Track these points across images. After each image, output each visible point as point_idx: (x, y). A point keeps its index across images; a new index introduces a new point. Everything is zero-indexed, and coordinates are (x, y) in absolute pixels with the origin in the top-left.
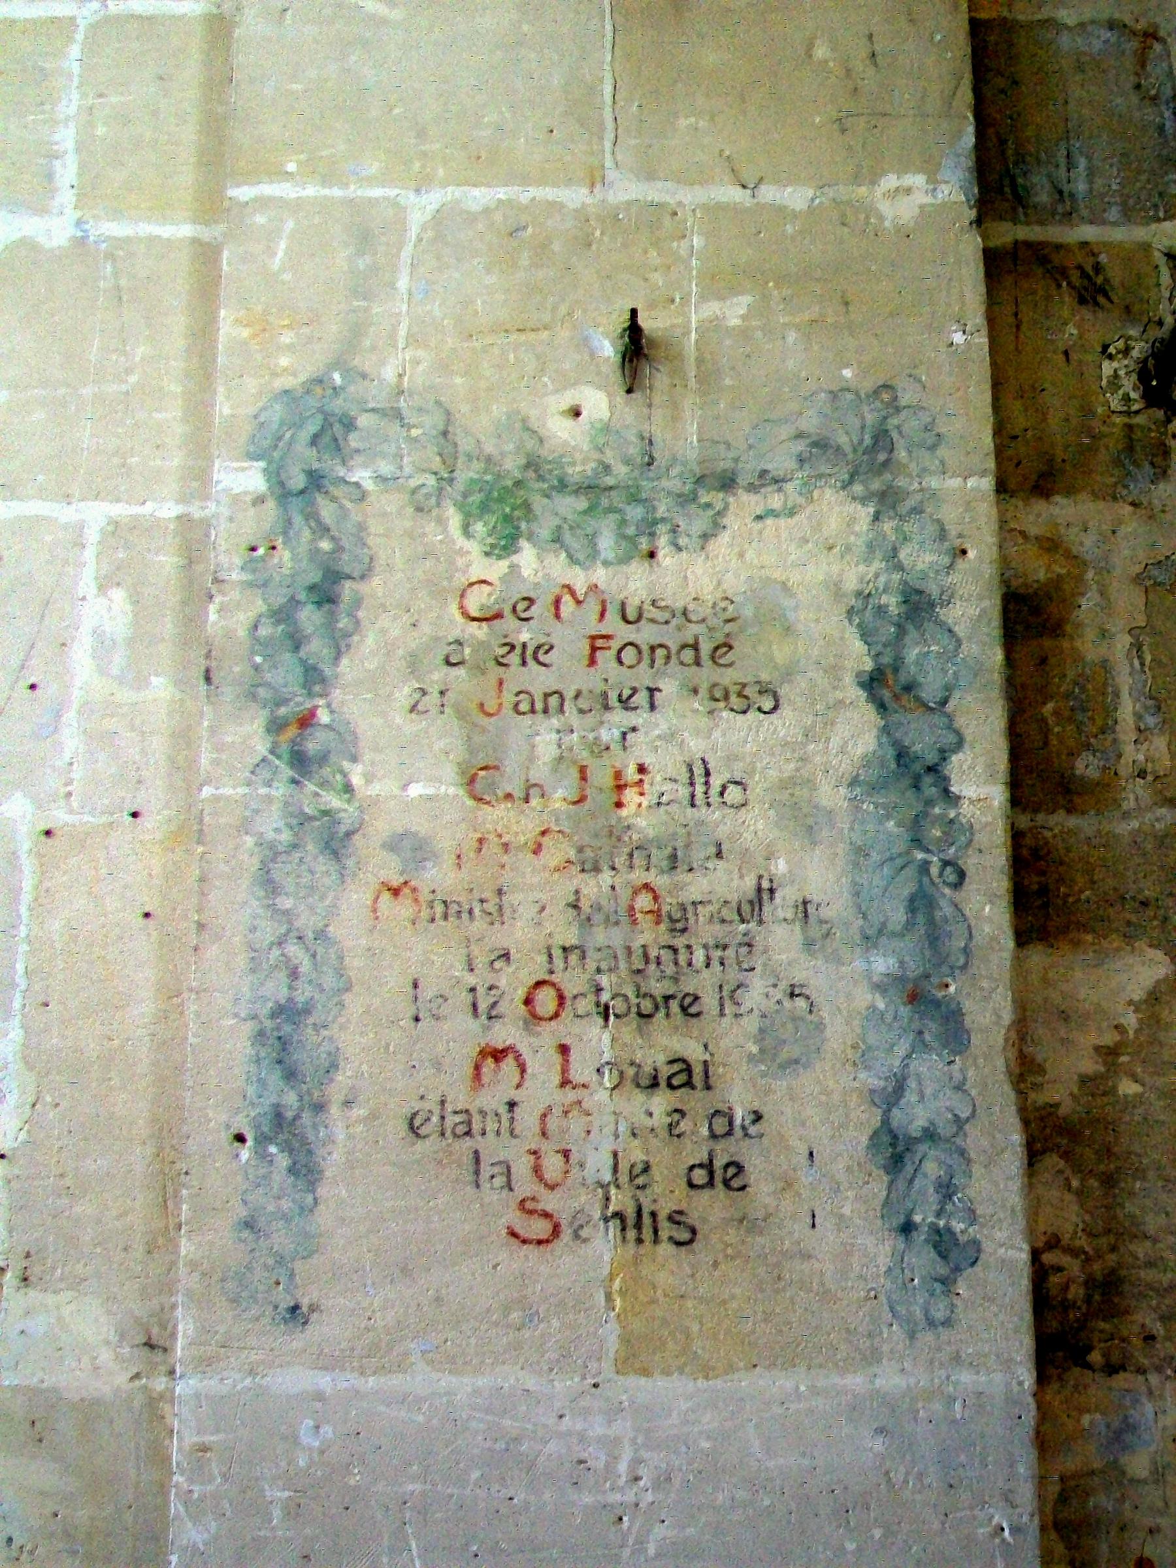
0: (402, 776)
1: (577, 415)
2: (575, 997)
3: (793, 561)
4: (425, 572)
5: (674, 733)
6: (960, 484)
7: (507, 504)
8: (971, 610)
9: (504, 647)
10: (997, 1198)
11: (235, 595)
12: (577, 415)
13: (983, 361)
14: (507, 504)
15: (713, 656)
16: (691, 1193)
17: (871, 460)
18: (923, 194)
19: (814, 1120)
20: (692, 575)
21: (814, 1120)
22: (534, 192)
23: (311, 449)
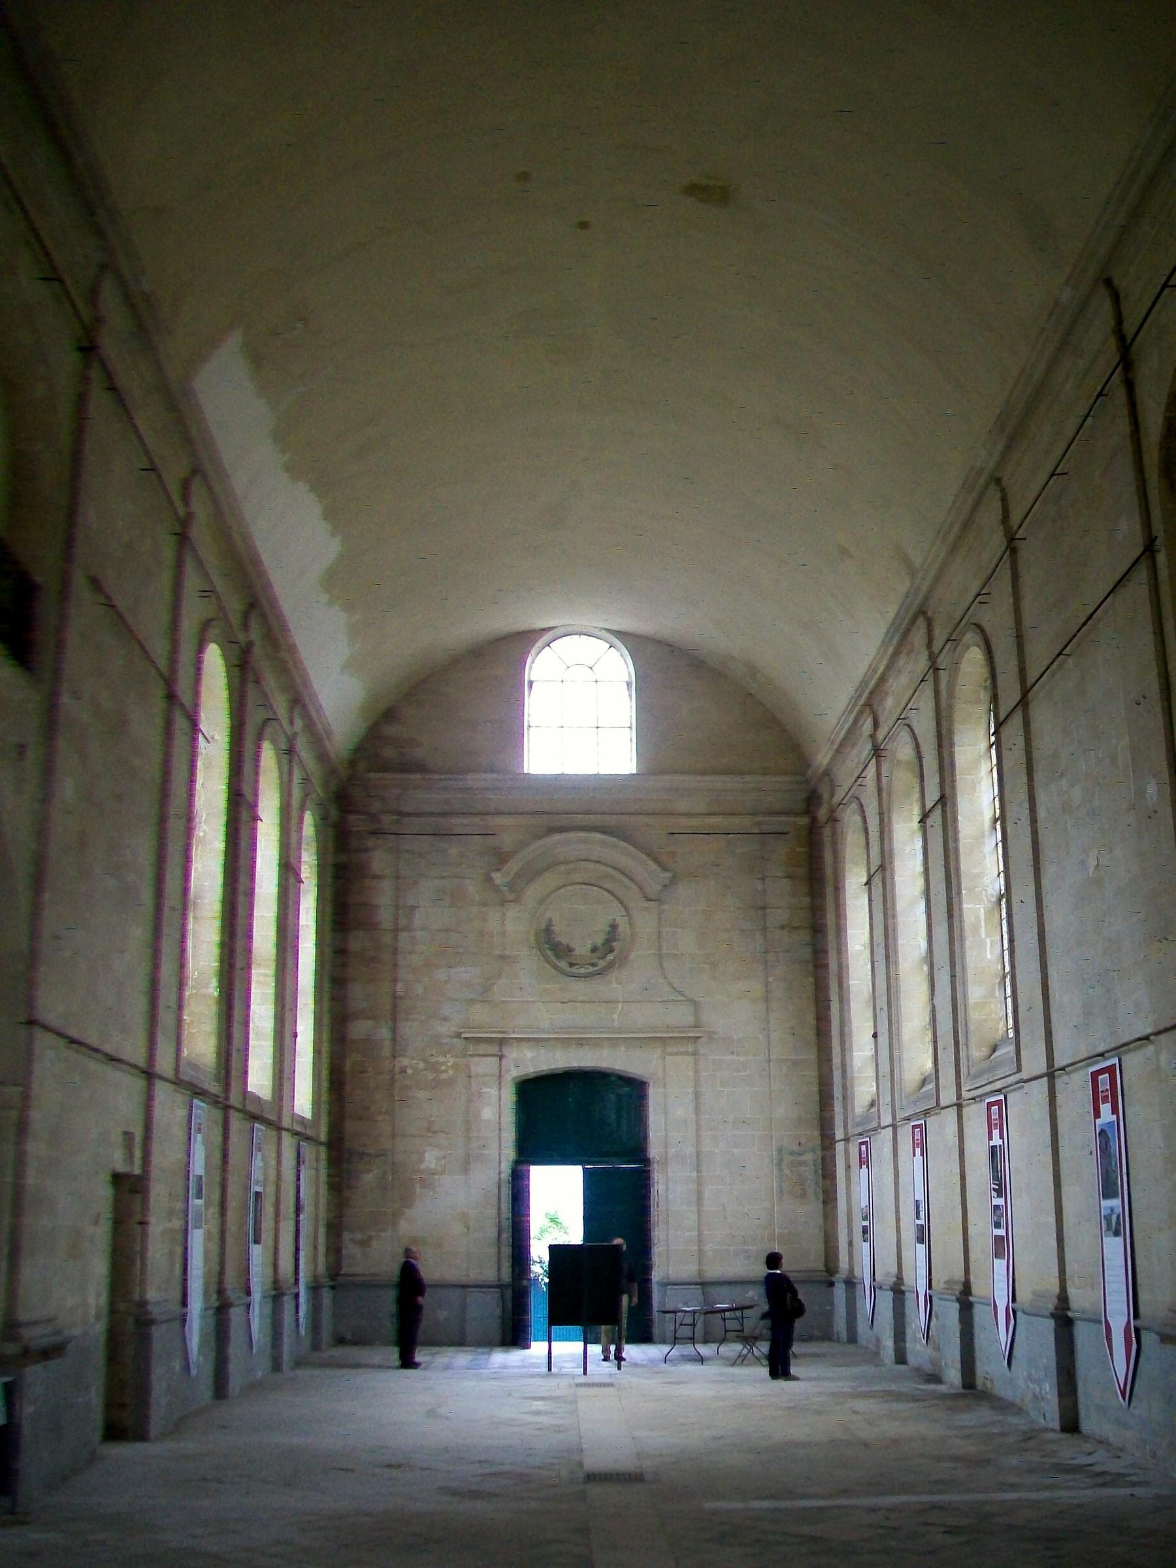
0: (787, 1172)
1: (796, 1148)
2: (909, 726)
3: (809, 1157)
4: (787, 1159)
5: (803, 1168)
6: (819, 1153)
7: (792, 1153)
8: (820, 1161)
9: (792, 1162)
10: (821, 1197)
11: (288, 1292)
12: (796, 1148)
13: (665, 1161)
14: (792, 1153)
15: (803, 1163)
16: (804, 1195)
17: (813, 1151)
18: (817, 1133)
19: (810, 1191)
20: (802, 1158)
21: (810, 1191)
22: (1074, 1493)
23: (780, 1150)
